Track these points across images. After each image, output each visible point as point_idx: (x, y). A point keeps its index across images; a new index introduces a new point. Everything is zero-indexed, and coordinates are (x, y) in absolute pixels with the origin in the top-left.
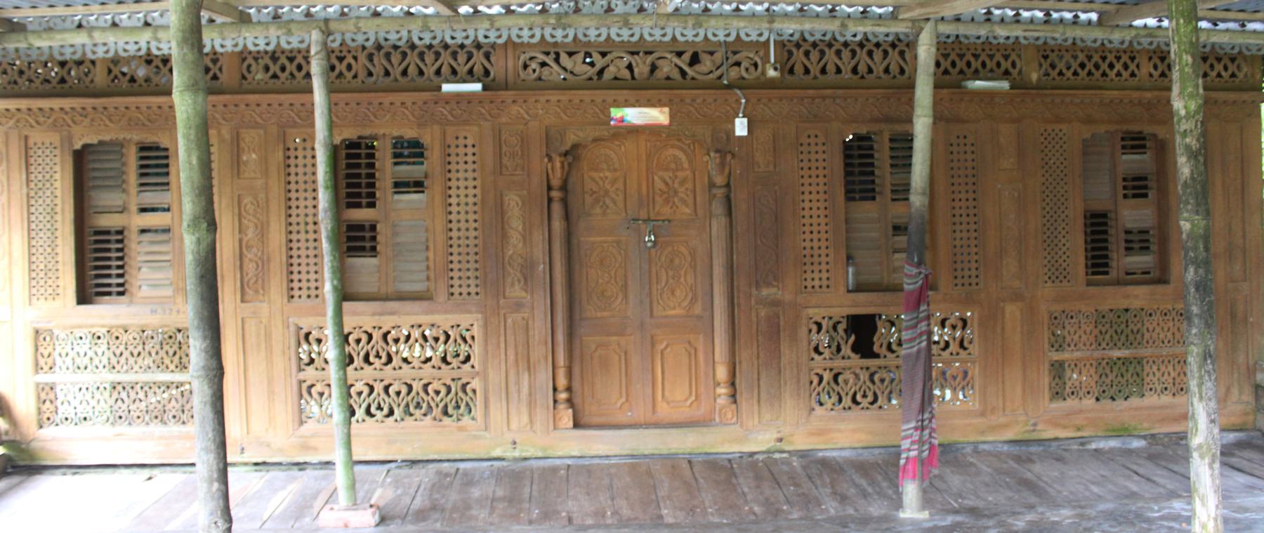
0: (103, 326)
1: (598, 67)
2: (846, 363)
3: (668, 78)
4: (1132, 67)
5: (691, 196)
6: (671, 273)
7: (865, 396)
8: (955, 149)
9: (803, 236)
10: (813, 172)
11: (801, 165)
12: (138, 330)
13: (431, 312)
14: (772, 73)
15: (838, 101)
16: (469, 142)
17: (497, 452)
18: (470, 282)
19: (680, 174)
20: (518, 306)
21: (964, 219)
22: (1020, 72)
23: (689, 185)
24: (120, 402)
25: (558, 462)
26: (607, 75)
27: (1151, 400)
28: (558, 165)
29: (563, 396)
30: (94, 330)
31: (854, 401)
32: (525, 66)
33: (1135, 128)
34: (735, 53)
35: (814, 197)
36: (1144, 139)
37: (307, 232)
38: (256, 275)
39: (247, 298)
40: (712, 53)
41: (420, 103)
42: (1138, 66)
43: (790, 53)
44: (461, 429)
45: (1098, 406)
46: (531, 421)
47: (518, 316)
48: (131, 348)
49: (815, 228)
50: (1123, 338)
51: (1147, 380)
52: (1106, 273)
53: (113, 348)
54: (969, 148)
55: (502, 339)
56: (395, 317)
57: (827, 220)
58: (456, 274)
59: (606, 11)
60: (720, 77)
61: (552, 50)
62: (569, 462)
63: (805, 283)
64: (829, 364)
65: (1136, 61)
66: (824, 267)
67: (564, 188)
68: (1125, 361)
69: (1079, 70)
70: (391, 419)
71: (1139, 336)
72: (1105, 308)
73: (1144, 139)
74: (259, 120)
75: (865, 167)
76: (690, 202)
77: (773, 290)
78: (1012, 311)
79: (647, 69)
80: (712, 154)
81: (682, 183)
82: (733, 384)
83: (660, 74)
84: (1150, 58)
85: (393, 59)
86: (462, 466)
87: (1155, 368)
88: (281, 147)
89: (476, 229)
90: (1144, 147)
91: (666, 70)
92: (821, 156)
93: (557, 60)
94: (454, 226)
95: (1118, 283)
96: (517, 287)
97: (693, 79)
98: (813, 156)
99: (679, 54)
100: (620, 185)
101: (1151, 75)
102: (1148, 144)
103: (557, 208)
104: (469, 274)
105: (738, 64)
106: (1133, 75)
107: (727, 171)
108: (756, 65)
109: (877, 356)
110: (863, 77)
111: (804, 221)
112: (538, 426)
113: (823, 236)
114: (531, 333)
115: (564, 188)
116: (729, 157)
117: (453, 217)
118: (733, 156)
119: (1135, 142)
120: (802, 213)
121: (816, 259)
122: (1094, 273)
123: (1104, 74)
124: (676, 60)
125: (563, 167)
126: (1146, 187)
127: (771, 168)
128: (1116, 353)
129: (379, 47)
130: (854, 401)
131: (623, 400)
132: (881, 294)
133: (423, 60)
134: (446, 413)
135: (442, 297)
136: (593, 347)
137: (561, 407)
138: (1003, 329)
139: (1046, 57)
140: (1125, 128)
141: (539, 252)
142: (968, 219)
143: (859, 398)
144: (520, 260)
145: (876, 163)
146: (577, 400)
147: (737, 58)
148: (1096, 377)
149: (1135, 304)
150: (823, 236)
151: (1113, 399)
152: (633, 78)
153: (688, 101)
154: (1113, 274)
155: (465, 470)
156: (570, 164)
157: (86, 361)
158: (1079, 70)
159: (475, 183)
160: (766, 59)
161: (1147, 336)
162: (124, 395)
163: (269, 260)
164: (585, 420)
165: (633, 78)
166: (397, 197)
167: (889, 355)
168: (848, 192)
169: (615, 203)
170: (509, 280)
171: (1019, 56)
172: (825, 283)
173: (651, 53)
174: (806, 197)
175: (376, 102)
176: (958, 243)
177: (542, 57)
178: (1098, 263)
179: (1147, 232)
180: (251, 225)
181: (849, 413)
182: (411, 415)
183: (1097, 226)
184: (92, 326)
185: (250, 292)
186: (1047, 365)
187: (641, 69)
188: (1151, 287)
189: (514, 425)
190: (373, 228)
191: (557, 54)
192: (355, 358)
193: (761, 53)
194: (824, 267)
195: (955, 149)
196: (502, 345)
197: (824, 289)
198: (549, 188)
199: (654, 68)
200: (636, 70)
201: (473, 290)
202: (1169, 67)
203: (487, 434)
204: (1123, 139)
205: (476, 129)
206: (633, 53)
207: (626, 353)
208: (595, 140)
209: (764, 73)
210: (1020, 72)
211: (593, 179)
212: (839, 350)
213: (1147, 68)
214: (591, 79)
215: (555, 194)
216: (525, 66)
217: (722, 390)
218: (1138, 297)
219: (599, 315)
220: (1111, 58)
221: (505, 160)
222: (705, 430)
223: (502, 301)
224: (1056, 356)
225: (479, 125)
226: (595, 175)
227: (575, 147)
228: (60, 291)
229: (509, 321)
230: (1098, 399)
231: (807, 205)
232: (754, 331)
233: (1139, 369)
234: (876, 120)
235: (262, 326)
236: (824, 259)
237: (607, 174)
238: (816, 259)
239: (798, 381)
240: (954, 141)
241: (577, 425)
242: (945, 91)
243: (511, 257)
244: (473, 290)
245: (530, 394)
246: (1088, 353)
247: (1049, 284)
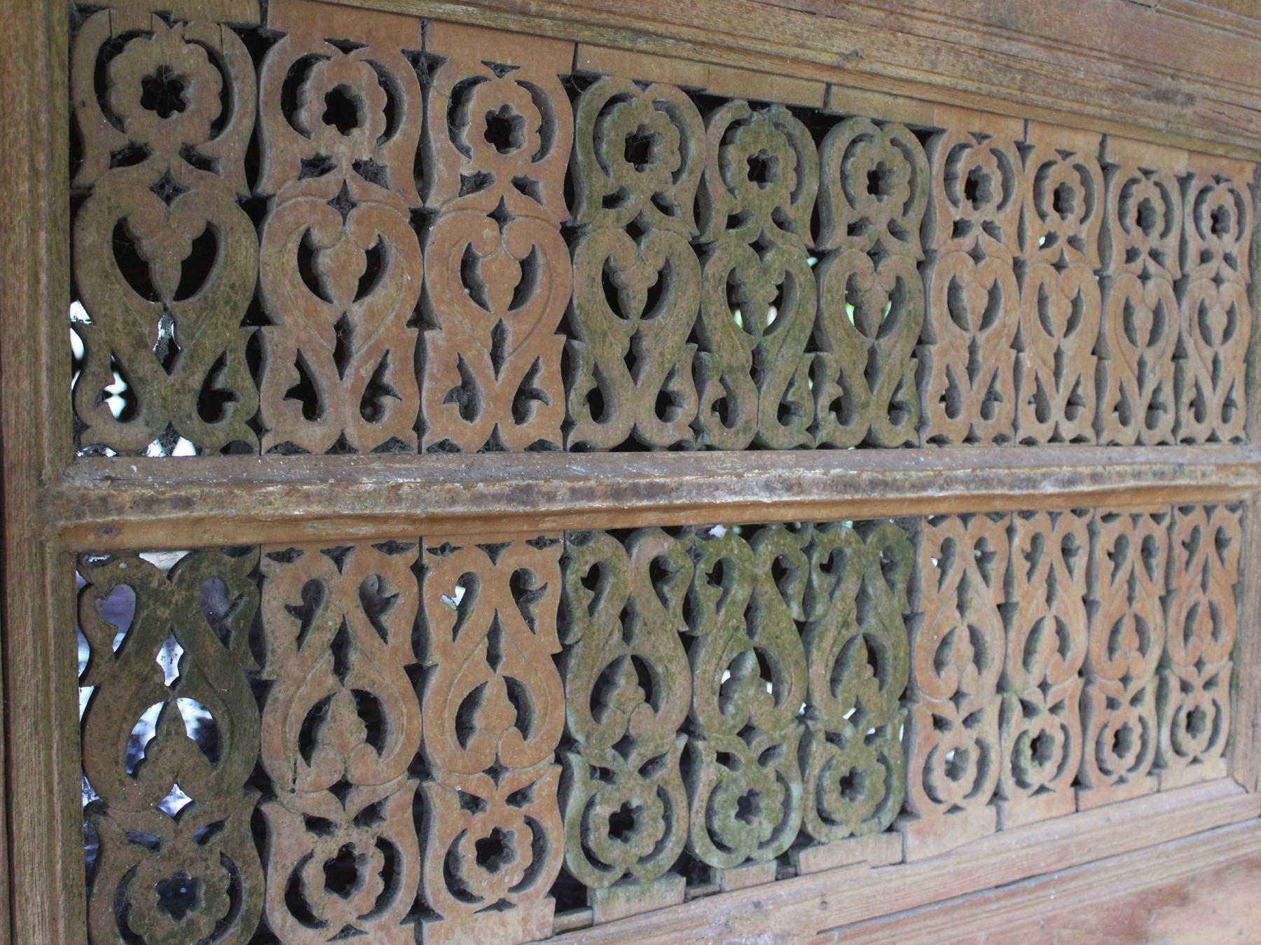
51: (934, 695)
148: (559, 707)
230: (569, 895)
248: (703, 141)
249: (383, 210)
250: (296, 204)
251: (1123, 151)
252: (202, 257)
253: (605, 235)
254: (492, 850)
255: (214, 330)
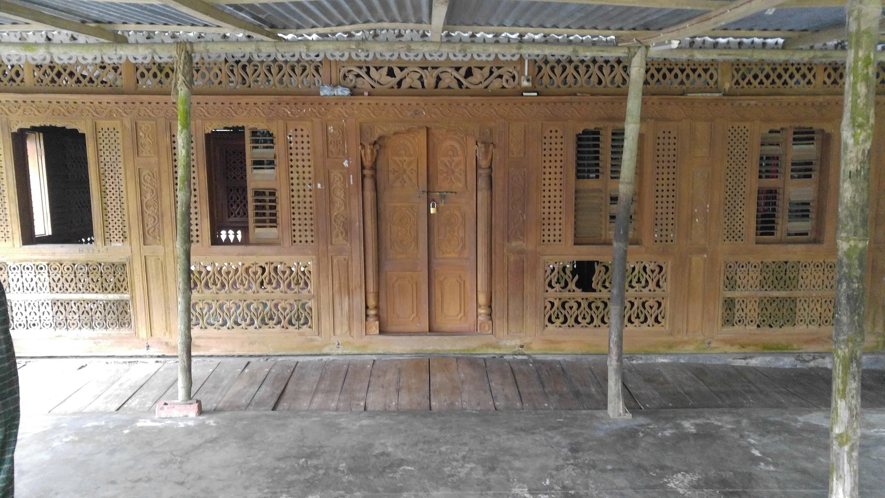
0: (44, 260)
1: (398, 79)
2: (572, 294)
3: (449, 87)
4: (810, 76)
5: (463, 174)
6: (448, 229)
7: (584, 318)
8: (661, 141)
9: (543, 205)
10: (553, 158)
11: (544, 152)
12: (70, 263)
13: (280, 254)
14: (525, 84)
15: (574, 105)
16: (305, 133)
17: (326, 350)
18: (307, 233)
19: (456, 159)
20: (340, 252)
21: (665, 193)
22: (716, 82)
23: (462, 167)
24: (59, 313)
25: (367, 357)
26: (405, 85)
27: (801, 328)
28: (369, 151)
29: (372, 312)
30: (37, 263)
31: (576, 321)
32: (345, 77)
33: (807, 125)
34: (499, 68)
35: (553, 176)
36: (813, 133)
37: (299, 196)
38: (154, 227)
39: (147, 242)
40: (481, 68)
41: (268, 104)
42: (814, 76)
43: (540, 69)
44: (301, 334)
45: (759, 331)
46: (350, 330)
47: (341, 258)
48: (65, 276)
49: (552, 199)
50: (782, 283)
51: (799, 313)
52: (772, 234)
53: (52, 276)
54: (672, 141)
55: (330, 273)
56: (254, 257)
57: (561, 193)
58: (297, 228)
59: (397, 37)
60: (486, 87)
61: (364, 65)
62: (375, 357)
63: (543, 238)
64: (559, 295)
65: (813, 72)
66: (557, 227)
67: (374, 168)
68: (783, 300)
69: (764, 80)
70: (252, 327)
71: (794, 282)
72: (768, 260)
73: (813, 133)
74: (151, 114)
75: (591, 152)
76: (462, 178)
77: (520, 243)
78: (697, 261)
79: (433, 81)
80: (479, 144)
81: (457, 165)
82: (490, 307)
83: (442, 84)
84: (825, 69)
85: (248, 70)
86: (280, 359)
87: (806, 306)
88: (168, 134)
89: (311, 196)
90: (812, 139)
91: (447, 81)
92: (559, 146)
93: (368, 73)
94: (295, 193)
95: (780, 242)
96: (341, 237)
97: (467, 88)
98: (553, 146)
99: (458, 69)
100: (414, 166)
101: (825, 83)
102: (815, 136)
103: (368, 183)
104: (306, 228)
105: (501, 76)
106: (809, 82)
107: (489, 157)
108: (514, 77)
109: (594, 291)
110: (570, 86)
111: (544, 194)
112: (354, 332)
113: (558, 204)
114: (350, 269)
115: (374, 168)
116: (491, 147)
117: (295, 187)
118: (495, 146)
119: (804, 135)
120: (543, 188)
121: (552, 221)
122: (762, 234)
123: (785, 83)
124: (455, 73)
125: (372, 153)
126: (810, 170)
127: (522, 155)
128: (776, 294)
129: (250, 61)
130: (576, 321)
131: (415, 315)
132: (599, 247)
133: (553, 72)
134: (290, 322)
135: (287, 242)
136: (395, 279)
137: (371, 319)
138: (690, 275)
139: (738, 71)
140: (797, 125)
141: (356, 214)
142: (668, 194)
143: (580, 319)
144: (342, 219)
145: (601, 150)
146: (383, 315)
147: (500, 72)
148: (758, 311)
149: (792, 258)
150: (558, 204)
151: (771, 326)
152: (423, 87)
153: (463, 105)
154: (778, 234)
155: (303, 363)
156: (377, 151)
157: (33, 284)
158: (764, 80)
159: (309, 163)
160: (521, 73)
161: (801, 281)
162: (62, 309)
163: (162, 216)
164: (391, 328)
165: (423, 87)
166: (255, 171)
167: (603, 290)
168: (578, 171)
169: (410, 180)
170: (334, 233)
171: (716, 69)
172: (557, 238)
173: (436, 68)
174: (547, 176)
175: (235, 102)
176: (659, 211)
177: (357, 71)
178: (766, 225)
179: (808, 204)
180: (149, 190)
181: (572, 329)
182: (266, 324)
183: (768, 202)
184: (36, 260)
185: (150, 238)
186: (721, 301)
187: (429, 81)
188: (810, 246)
189: (338, 332)
190: (273, 194)
191: (368, 68)
192: (198, 283)
193: (518, 68)
194: (557, 227)
195: (661, 141)
196: (330, 277)
197: (557, 242)
198: (363, 168)
199: (439, 79)
200: (425, 81)
201: (309, 239)
202: (841, 76)
203: (318, 338)
204: (795, 133)
205: (309, 123)
206: (423, 68)
207: (417, 283)
208: (395, 133)
209: (519, 84)
210: (716, 82)
211: (395, 162)
212: (566, 284)
213: (822, 76)
214: (393, 88)
215: (367, 172)
216: (345, 77)
217: (482, 311)
218: (796, 253)
219: (399, 257)
220: (792, 69)
221: (331, 147)
222: (469, 337)
223: (330, 247)
224: (729, 294)
225: (312, 121)
226: (397, 159)
227: (381, 138)
228: (10, 235)
229: (335, 261)
230: (758, 326)
231: (547, 182)
232: (506, 270)
233: (792, 306)
234: (604, 119)
235: (160, 262)
236: (557, 221)
237: (405, 158)
238: (552, 221)
239: (536, 307)
240: (661, 135)
241: (382, 332)
242: (656, 97)
243: (336, 216)
244: (309, 239)
245: (349, 310)
246: (753, 293)
247: (727, 241)
248: (773, 266)
249: (19, 276)
250: (739, 273)
251: (827, 261)
252: (72, 280)
253: (764, 274)
254: (813, 321)
255: (732, 283)
